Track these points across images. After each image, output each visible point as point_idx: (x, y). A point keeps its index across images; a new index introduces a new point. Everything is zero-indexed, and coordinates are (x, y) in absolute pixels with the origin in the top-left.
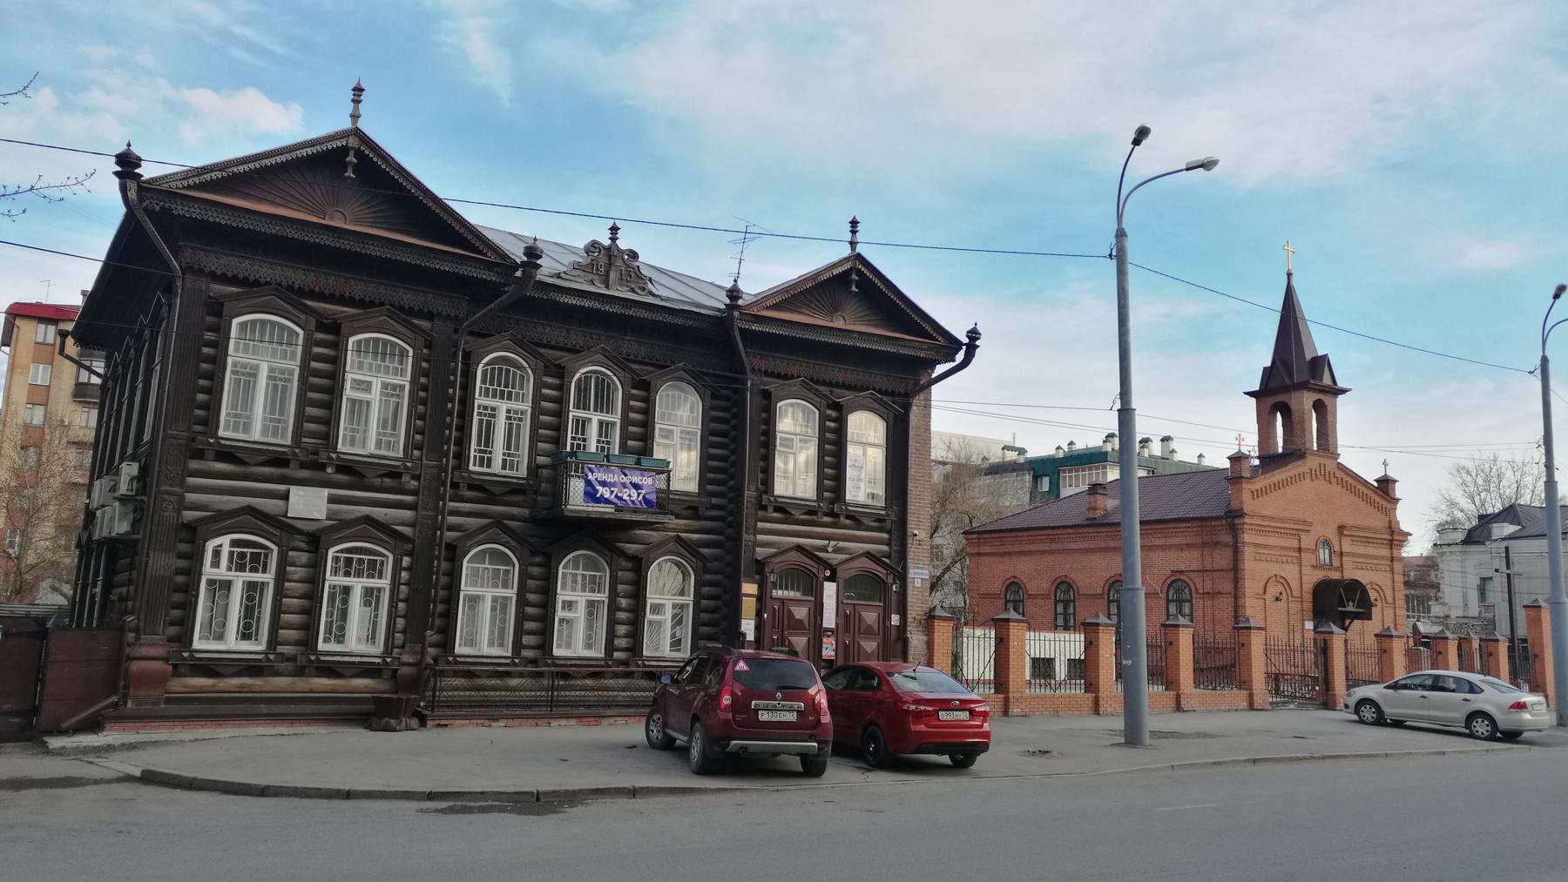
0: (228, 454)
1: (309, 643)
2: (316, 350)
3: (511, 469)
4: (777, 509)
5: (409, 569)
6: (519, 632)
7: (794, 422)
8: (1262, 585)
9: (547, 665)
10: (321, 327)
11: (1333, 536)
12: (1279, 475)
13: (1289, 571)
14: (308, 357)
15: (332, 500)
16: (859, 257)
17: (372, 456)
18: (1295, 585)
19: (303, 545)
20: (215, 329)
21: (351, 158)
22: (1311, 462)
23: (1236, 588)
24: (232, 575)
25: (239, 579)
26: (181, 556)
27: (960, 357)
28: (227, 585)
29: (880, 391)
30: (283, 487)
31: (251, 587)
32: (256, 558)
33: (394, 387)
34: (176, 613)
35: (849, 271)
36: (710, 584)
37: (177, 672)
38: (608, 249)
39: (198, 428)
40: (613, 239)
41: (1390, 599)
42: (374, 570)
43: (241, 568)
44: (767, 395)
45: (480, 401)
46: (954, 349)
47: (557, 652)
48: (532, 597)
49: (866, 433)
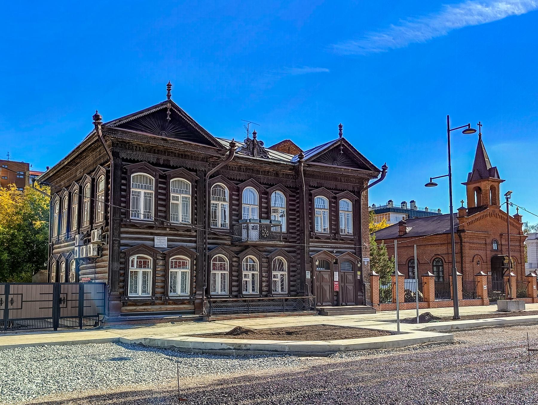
1: (165, 293)
5: (196, 265)
6: (231, 286)
7: (321, 202)
8: (472, 259)
9: (241, 298)
11: (498, 239)
12: (478, 215)
13: (482, 253)
15: (169, 240)
17: (181, 224)
18: (484, 258)
21: (169, 112)
22: (489, 210)
23: (462, 260)
25: (141, 271)
26: (121, 263)
27: (379, 176)
30: (152, 237)
31: (144, 273)
34: (121, 284)
35: (340, 145)
36: (293, 266)
37: (124, 305)
39: (122, 216)
40: (255, 137)
41: (519, 262)
42: (184, 265)
46: (378, 173)
47: (244, 293)
49: (346, 206)
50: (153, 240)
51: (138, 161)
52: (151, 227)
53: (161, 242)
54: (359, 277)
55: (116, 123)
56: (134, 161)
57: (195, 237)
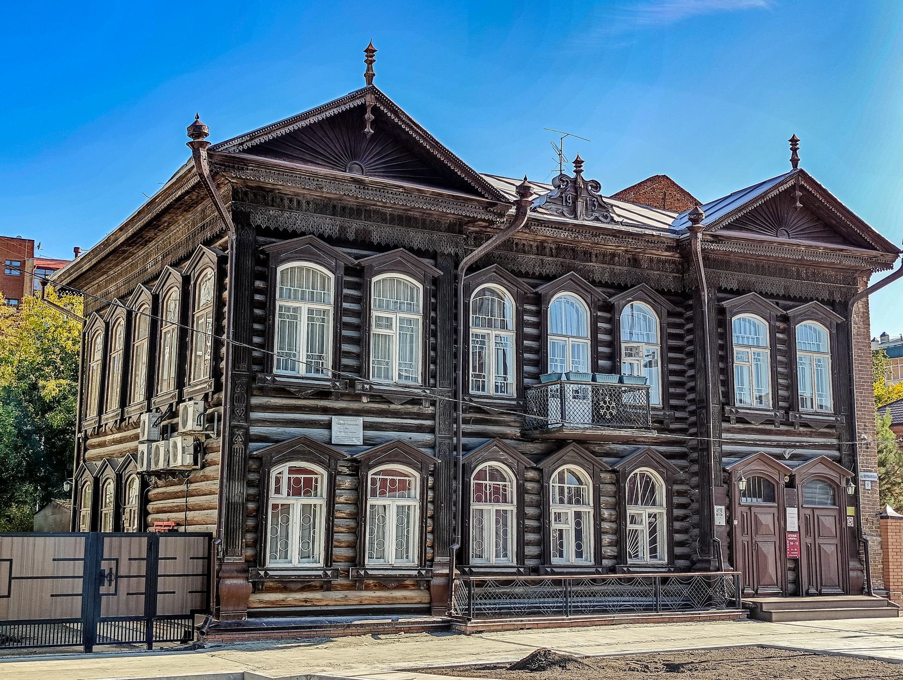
0: (282, 391)
2: (346, 291)
3: (317, 371)
4: (740, 420)
6: (521, 544)
9: (547, 573)
10: (349, 271)
14: (340, 298)
15: (366, 426)
16: (373, 90)
17: (397, 385)
19: (346, 470)
20: (262, 277)
21: (369, 116)
24: (291, 501)
26: (250, 484)
28: (286, 508)
29: (761, 293)
30: (325, 418)
32: (308, 482)
33: (410, 321)
34: (249, 536)
35: (793, 187)
36: (680, 494)
37: (257, 587)
38: (575, 181)
39: (256, 368)
40: (578, 172)
43: (297, 493)
44: (722, 311)
45: (473, 330)
48: (530, 511)
50: (328, 426)
51: (294, 234)
52: (323, 394)
53: (348, 431)
54: (850, 522)
55: (242, 144)
56: (285, 234)
57: (432, 417)
